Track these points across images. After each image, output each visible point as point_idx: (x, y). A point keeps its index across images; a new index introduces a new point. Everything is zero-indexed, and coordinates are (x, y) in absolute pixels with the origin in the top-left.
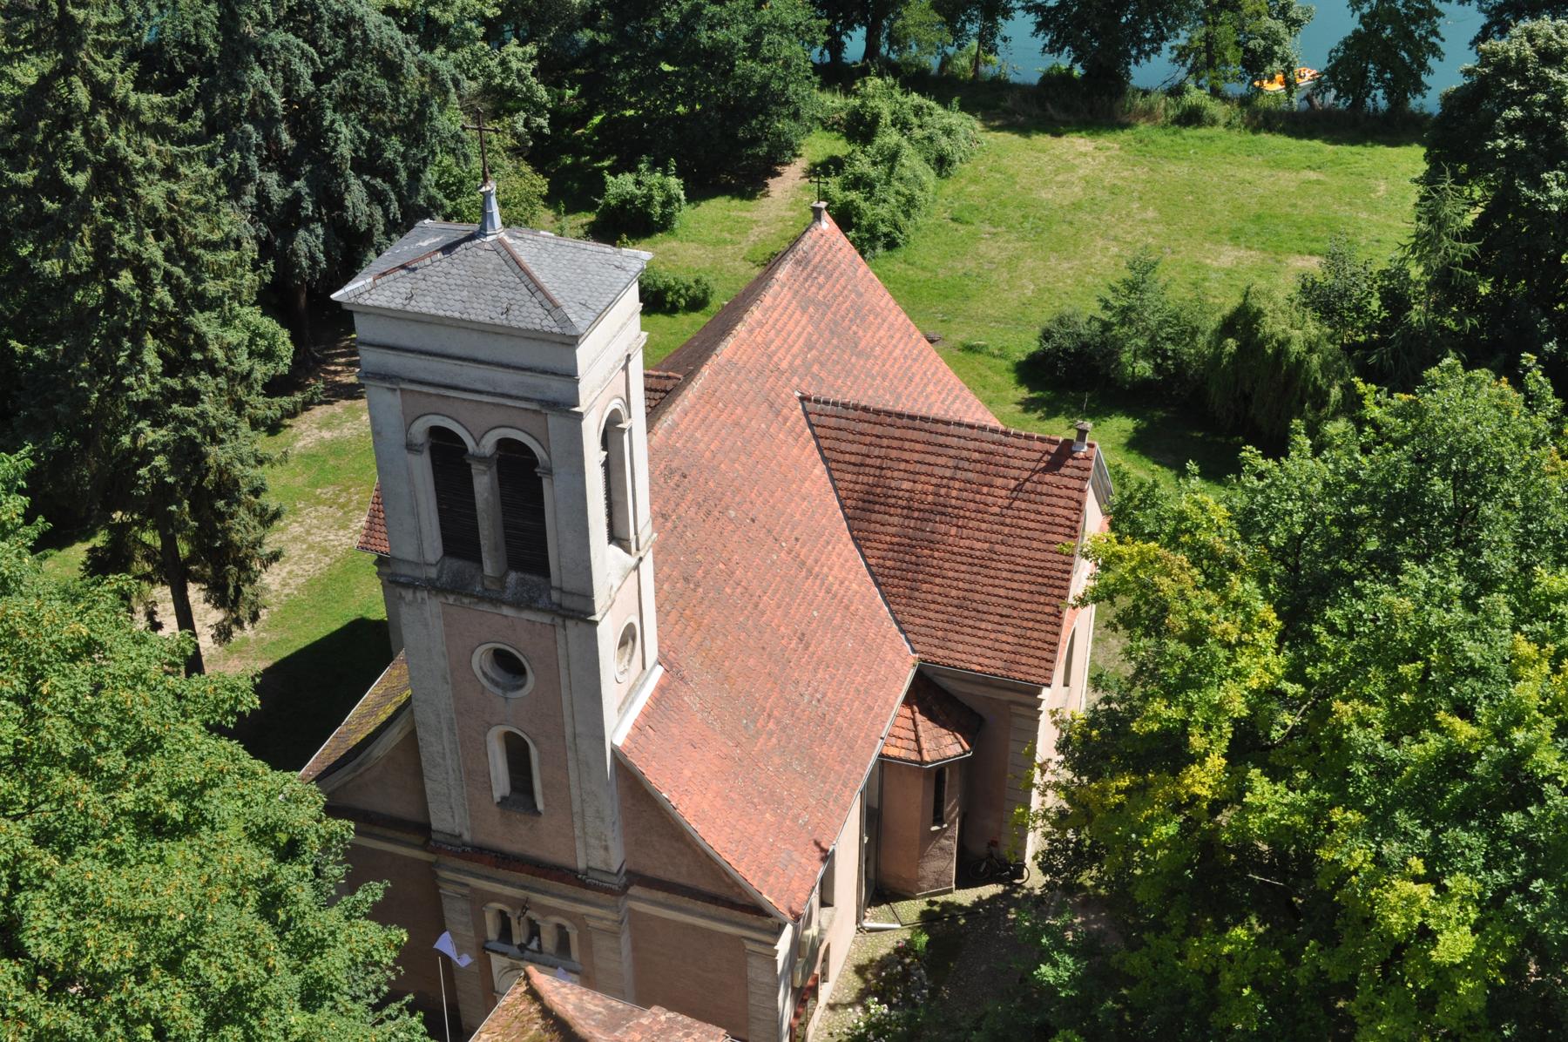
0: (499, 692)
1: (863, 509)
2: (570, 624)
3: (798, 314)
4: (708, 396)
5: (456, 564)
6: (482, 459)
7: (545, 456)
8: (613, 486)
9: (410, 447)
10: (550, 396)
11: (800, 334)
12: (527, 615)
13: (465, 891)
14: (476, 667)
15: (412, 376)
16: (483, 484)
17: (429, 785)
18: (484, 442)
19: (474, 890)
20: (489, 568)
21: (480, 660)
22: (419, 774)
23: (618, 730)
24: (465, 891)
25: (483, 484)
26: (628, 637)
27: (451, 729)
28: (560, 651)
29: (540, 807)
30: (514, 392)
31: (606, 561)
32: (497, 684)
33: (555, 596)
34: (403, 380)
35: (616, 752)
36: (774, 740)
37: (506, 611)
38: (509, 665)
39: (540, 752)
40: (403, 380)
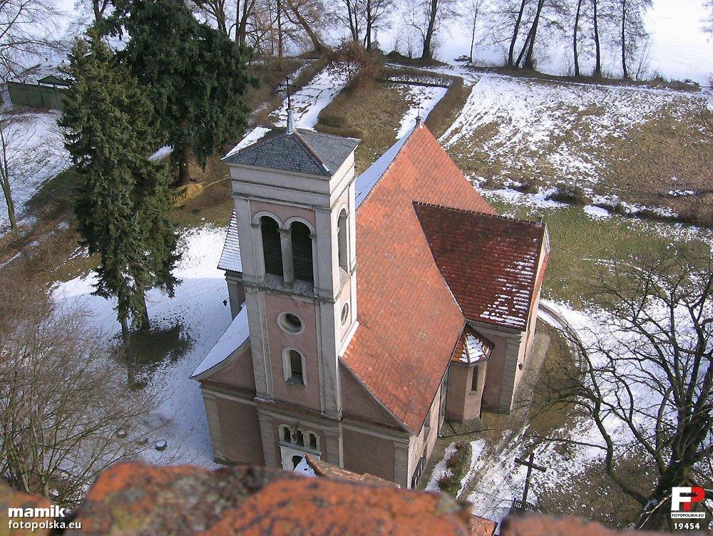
5: (272, 277)
16: (285, 242)
17: (264, 445)
22: (251, 368)
25: (285, 242)
29: (305, 383)
38: (293, 321)
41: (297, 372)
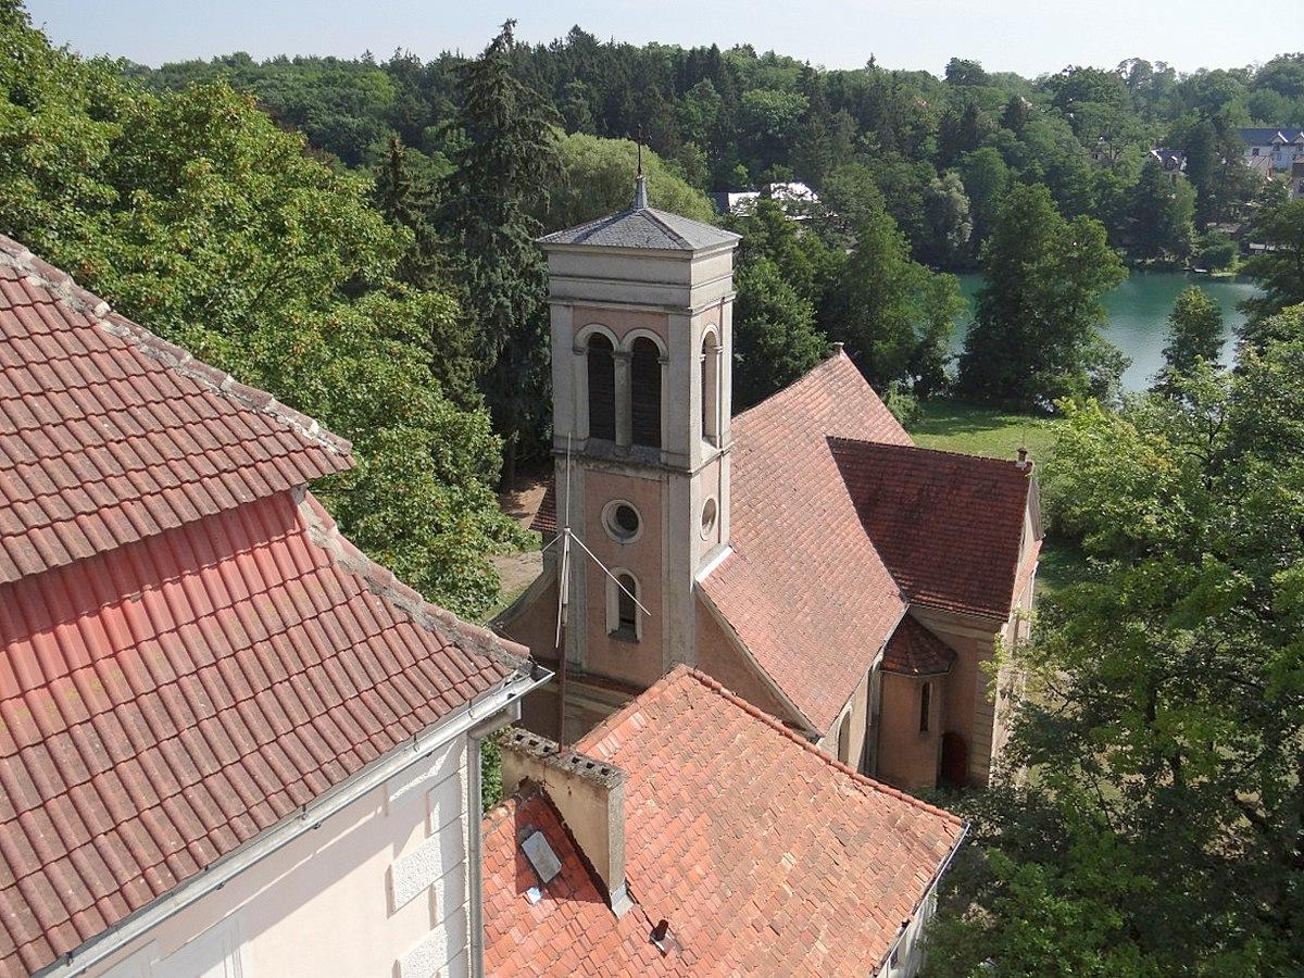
0: (618, 539)
1: (869, 509)
2: (672, 478)
3: (825, 395)
4: (767, 416)
5: (598, 442)
6: (621, 354)
7: (665, 349)
8: (707, 395)
9: (576, 350)
10: (673, 300)
11: (826, 407)
12: (644, 474)
13: (579, 713)
14: (604, 522)
15: (581, 296)
16: (621, 373)
18: (624, 342)
19: (586, 711)
20: (619, 441)
21: (608, 515)
23: (701, 574)
24: (579, 713)
25: (621, 373)
26: (709, 517)
27: (582, 573)
28: (663, 503)
29: (639, 636)
30: (647, 301)
31: (701, 451)
32: (617, 534)
33: (663, 457)
34: (575, 299)
35: (697, 587)
36: (808, 618)
37: (629, 472)
39: (645, 526)
40: (575, 299)
41: (627, 619)
